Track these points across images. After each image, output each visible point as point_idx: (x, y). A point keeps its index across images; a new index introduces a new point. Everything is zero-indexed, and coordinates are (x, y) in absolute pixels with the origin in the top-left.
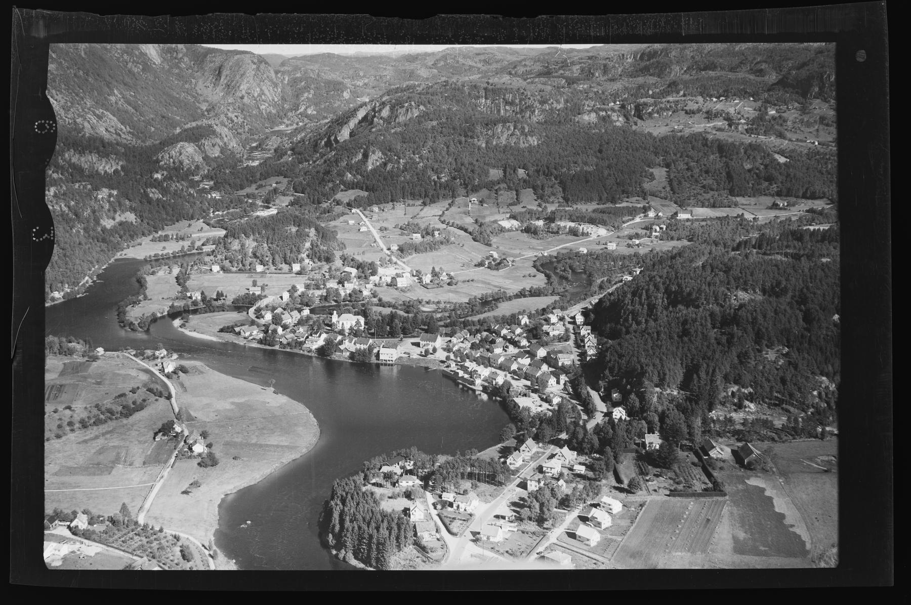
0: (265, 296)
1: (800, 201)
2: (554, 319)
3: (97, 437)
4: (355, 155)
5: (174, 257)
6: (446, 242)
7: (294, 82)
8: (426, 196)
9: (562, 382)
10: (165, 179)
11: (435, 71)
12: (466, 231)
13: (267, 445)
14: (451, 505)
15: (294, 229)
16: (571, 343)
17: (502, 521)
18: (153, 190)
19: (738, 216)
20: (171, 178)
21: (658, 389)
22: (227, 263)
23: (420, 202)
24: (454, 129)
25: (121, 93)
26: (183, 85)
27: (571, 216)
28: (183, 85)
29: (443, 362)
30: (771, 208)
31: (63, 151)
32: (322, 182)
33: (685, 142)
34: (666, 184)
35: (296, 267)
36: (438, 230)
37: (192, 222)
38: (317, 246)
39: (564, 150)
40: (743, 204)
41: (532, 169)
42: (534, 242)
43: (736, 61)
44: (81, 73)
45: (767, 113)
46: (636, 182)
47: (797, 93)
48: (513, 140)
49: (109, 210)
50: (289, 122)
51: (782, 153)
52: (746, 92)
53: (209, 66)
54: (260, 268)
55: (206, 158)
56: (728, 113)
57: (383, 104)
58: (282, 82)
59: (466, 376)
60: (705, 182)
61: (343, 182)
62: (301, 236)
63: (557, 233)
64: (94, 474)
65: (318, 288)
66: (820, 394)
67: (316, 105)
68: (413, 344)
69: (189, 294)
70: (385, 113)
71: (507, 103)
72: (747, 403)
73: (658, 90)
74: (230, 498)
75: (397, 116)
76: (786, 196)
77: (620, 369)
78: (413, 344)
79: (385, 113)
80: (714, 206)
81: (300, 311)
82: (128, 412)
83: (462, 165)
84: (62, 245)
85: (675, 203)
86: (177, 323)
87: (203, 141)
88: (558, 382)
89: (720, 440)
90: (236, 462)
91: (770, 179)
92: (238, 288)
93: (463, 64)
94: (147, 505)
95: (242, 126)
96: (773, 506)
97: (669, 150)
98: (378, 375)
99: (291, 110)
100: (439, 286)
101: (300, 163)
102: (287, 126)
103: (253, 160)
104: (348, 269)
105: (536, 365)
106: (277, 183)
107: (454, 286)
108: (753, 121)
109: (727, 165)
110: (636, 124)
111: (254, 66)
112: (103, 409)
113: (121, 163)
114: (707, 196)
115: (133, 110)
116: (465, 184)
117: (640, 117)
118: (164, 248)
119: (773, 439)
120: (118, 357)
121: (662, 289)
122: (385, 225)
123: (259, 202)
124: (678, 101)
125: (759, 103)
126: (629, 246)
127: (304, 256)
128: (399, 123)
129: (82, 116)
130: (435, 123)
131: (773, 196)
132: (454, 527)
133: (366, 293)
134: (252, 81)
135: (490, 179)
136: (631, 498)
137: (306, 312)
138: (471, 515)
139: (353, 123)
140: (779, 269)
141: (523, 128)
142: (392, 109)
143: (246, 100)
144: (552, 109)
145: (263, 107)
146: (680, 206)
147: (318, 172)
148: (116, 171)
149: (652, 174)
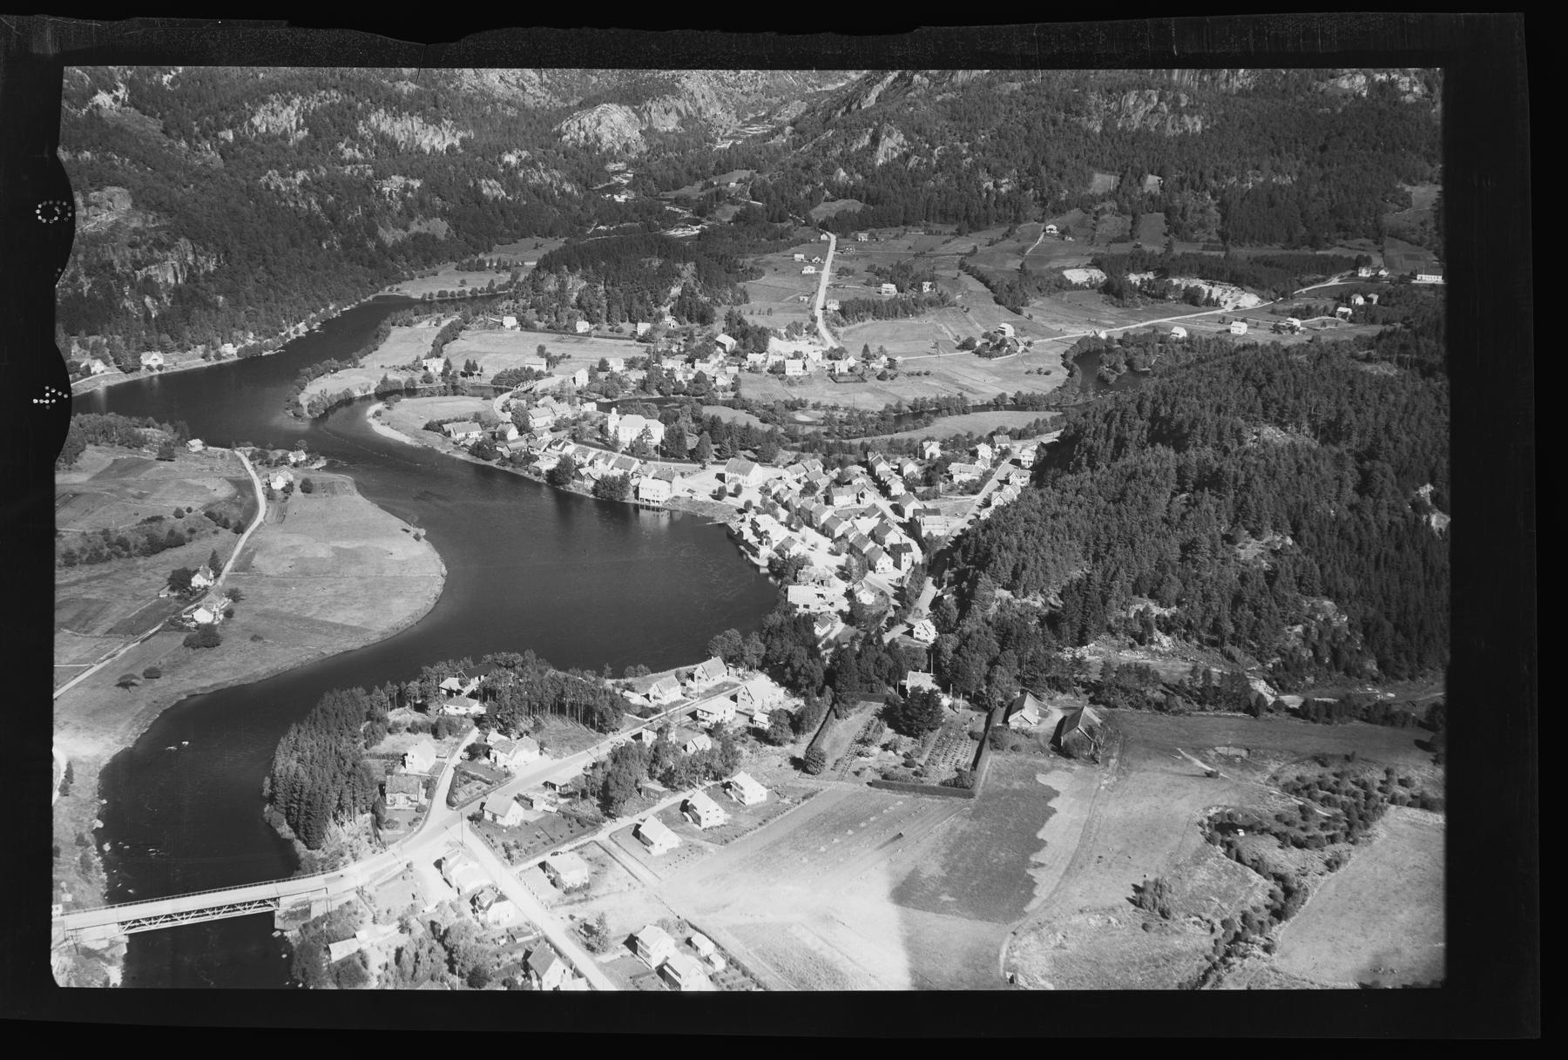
0: (550, 375)
3: (76, 583)
4: (857, 137)
5: (474, 298)
10: (524, 163)
12: (987, 284)
18: (492, 182)
20: (533, 164)
23: (953, 229)
24: (1048, 97)
27: (1202, 268)
31: (368, 112)
35: (643, 328)
38: (693, 294)
46: (1369, 210)
48: (1154, 122)
49: (400, 214)
54: (582, 326)
55: (648, 133)
61: (829, 185)
66: (1307, 630)
72: (1157, 635)
74: (193, 701)
77: (977, 550)
87: (649, 104)
88: (897, 565)
90: (250, 645)
116: (1042, 198)
120: (222, 456)
121: (1147, 413)
127: (665, 309)
135: (1091, 191)
138: (507, 774)
141: (1177, 100)
147: (795, 165)
148: (451, 148)
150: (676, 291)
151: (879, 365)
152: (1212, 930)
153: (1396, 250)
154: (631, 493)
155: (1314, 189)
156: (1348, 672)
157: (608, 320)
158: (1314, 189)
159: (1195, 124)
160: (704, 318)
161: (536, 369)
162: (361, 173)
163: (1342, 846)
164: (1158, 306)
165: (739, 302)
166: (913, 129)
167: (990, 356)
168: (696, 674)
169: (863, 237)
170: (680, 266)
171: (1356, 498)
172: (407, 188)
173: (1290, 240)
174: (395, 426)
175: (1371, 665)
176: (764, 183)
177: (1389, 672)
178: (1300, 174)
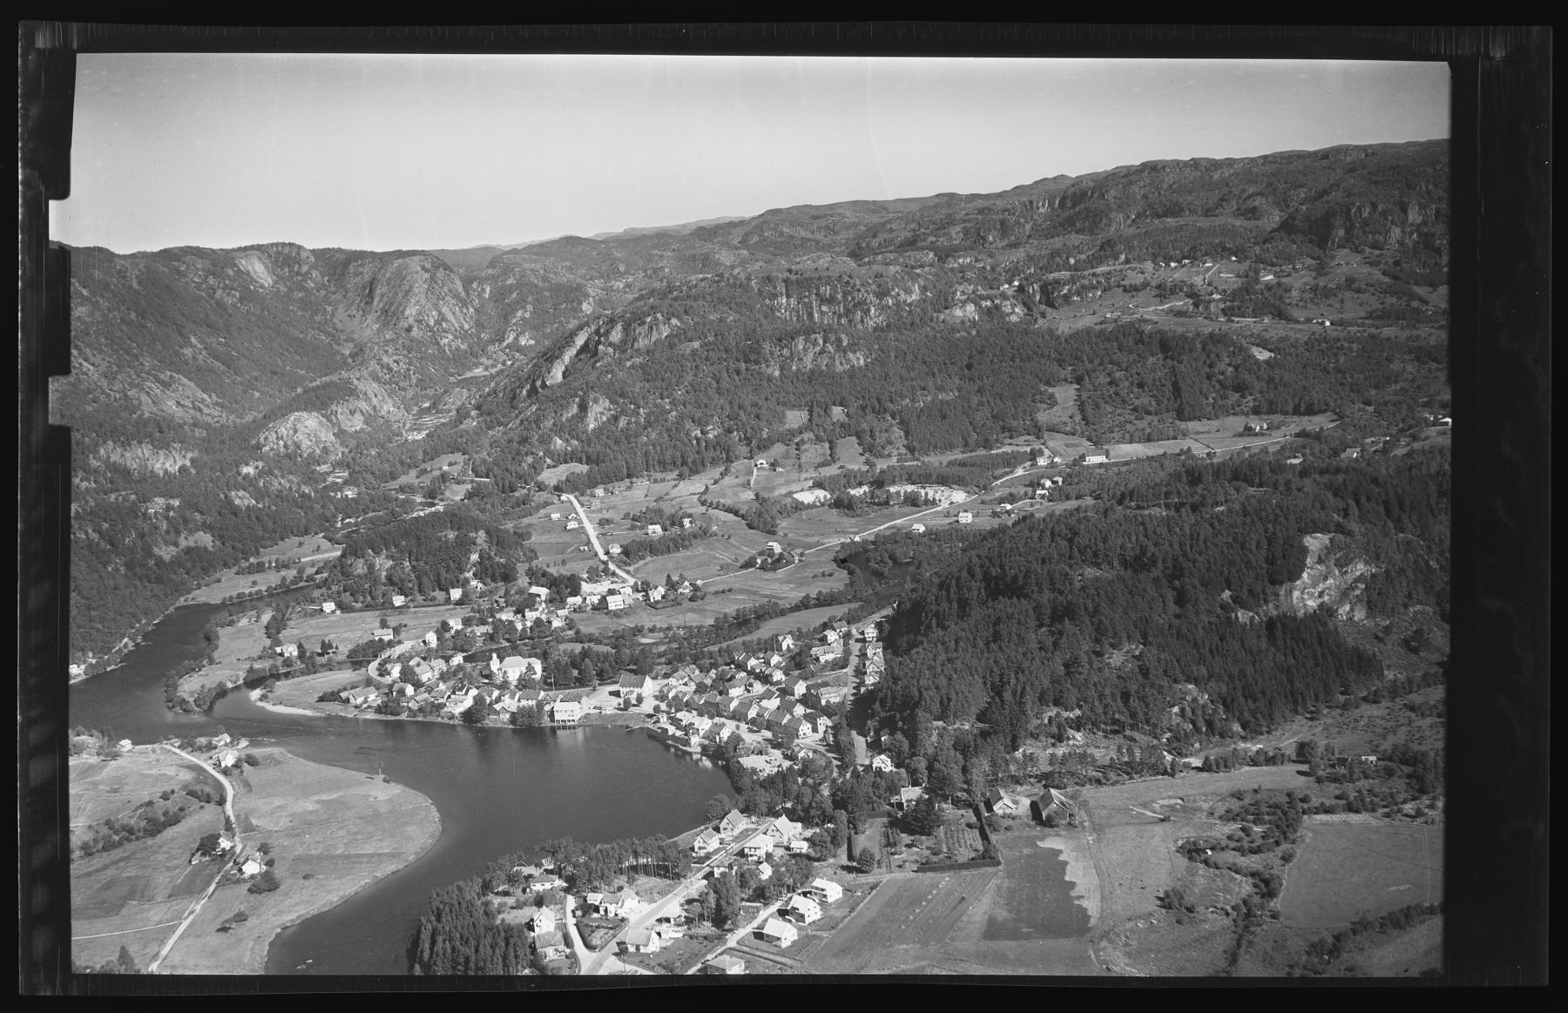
0: (400, 642)
1: (1289, 419)
2: (832, 636)
3: (106, 867)
4: (566, 407)
5: (271, 595)
6: (703, 534)
7: (500, 295)
8: (684, 463)
9: (821, 729)
10: (261, 473)
11: (745, 252)
12: (736, 513)
13: (358, 856)
14: (597, 909)
15: (452, 535)
16: (849, 670)
17: (665, 925)
18: (241, 493)
19: (1182, 452)
21: (940, 723)
22: (347, 598)
23: (674, 475)
24: (727, 351)
25: (202, 342)
26: (312, 317)
28: (312, 317)
29: (650, 716)
30: (1241, 435)
31: (97, 445)
32: (518, 456)
33: (1108, 340)
34: (1075, 410)
35: (456, 594)
36: (690, 516)
37: (306, 539)
39: (909, 369)
40: (1198, 433)
41: (854, 406)
42: (847, 522)
43: (1215, 196)
44: (133, 315)
45: (1257, 281)
47: (1311, 241)
49: (168, 532)
50: (490, 362)
51: (1264, 345)
52: (1224, 249)
53: (353, 282)
54: (399, 601)
55: (341, 434)
56: (1192, 286)
57: (612, 322)
58: (480, 296)
59: (679, 733)
60: (1137, 402)
61: (548, 453)
62: (465, 545)
63: (886, 503)
64: (95, 917)
65: (483, 622)
66: (1182, 710)
67: (536, 328)
68: (611, 693)
69: (278, 650)
70: (616, 335)
71: (823, 300)
72: (1071, 732)
73: (1083, 257)
74: (289, 931)
75: (635, 340)
76: (1270, 412)
77: (894, 698)
78: (611, 693)
79: (616, 335)
80: (1149, 439)
81: (447, 659)
82: (155, 827)
83: (740, 407)
84: (85, 592)
85: (1089, 439)
86: (255, 694)
88: (815, 730)
89: (1019, 788)
90: (307, 882)
91: (1241, 388)
92: (359, 634)
93: (792, 237)
94: (164, 952)
95: (406, 376)
96: (1064, 873)
97: (1081, 357)
98: (556, 744)
99: (492, 342)
100: (677, 603)
101: (489, 428)
102: (486, 369)
103: (419, 430)
104: (534, 590)
105: (786, 707)
106: (450, 464)
107: (700, 602)
108: (1234, 295)
109: (1173, 371)
110: (1043, 315)
111: (427, 276)
112: (117, 826)
113: (190, 455)
114: (1140, 424)
115: (222, 367)
117: (1051, 304)
118: (254, 583)
119: (1098, 782)
122: (606, 515)
123: (419, 499)
124: (1109, 273)
125: (1246, 265)
126: (995, 514)
127: (469, 575)
128: (638, 350)
129: (136, 386)
130: (696, 344)
131: (1247, 415)
132: (596, 940)
133: (557, 623)
134: (423, 301)
135: (787, 426)
136: (863, 879)
137: (458, 659)
138: (623, 920)
139: (568, 355)
140: (1146, 529)
141: (839, 340)
142: (626, 329)
143: (415, 332)
144: (897, 304)
145: (446, 341)
146: (1095, 444)
147: (510, 441)
148: (183, 469)
149: (1052, 396)
150: (474, 557)
151: (686, 589)
152: (1227, 914)
153: (1056, 442)
154: (546, 718)
155: (975, 400)
156: (1222, 736)
157: (420, 591)
158: (975, 400)
159: (858, 359)
160: (508, 577)
161: (386, 638)
162: (125, 499)
163: (1285, 846)
164: (886, 511)
165: (530, 560)
166: (617, 394)
167: (775, 570)
168: (722, 826)
169: (600, 492)
170: (472, 535)
171: (1178, 610)
172: (169, 508)
173: (966, 444)
174: (290, 701)
175: (1237, 727)
176: (485, 461)
177: (1251, 730)
178: (959, 390)
